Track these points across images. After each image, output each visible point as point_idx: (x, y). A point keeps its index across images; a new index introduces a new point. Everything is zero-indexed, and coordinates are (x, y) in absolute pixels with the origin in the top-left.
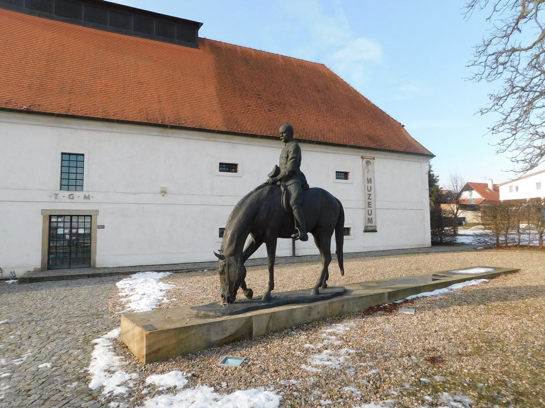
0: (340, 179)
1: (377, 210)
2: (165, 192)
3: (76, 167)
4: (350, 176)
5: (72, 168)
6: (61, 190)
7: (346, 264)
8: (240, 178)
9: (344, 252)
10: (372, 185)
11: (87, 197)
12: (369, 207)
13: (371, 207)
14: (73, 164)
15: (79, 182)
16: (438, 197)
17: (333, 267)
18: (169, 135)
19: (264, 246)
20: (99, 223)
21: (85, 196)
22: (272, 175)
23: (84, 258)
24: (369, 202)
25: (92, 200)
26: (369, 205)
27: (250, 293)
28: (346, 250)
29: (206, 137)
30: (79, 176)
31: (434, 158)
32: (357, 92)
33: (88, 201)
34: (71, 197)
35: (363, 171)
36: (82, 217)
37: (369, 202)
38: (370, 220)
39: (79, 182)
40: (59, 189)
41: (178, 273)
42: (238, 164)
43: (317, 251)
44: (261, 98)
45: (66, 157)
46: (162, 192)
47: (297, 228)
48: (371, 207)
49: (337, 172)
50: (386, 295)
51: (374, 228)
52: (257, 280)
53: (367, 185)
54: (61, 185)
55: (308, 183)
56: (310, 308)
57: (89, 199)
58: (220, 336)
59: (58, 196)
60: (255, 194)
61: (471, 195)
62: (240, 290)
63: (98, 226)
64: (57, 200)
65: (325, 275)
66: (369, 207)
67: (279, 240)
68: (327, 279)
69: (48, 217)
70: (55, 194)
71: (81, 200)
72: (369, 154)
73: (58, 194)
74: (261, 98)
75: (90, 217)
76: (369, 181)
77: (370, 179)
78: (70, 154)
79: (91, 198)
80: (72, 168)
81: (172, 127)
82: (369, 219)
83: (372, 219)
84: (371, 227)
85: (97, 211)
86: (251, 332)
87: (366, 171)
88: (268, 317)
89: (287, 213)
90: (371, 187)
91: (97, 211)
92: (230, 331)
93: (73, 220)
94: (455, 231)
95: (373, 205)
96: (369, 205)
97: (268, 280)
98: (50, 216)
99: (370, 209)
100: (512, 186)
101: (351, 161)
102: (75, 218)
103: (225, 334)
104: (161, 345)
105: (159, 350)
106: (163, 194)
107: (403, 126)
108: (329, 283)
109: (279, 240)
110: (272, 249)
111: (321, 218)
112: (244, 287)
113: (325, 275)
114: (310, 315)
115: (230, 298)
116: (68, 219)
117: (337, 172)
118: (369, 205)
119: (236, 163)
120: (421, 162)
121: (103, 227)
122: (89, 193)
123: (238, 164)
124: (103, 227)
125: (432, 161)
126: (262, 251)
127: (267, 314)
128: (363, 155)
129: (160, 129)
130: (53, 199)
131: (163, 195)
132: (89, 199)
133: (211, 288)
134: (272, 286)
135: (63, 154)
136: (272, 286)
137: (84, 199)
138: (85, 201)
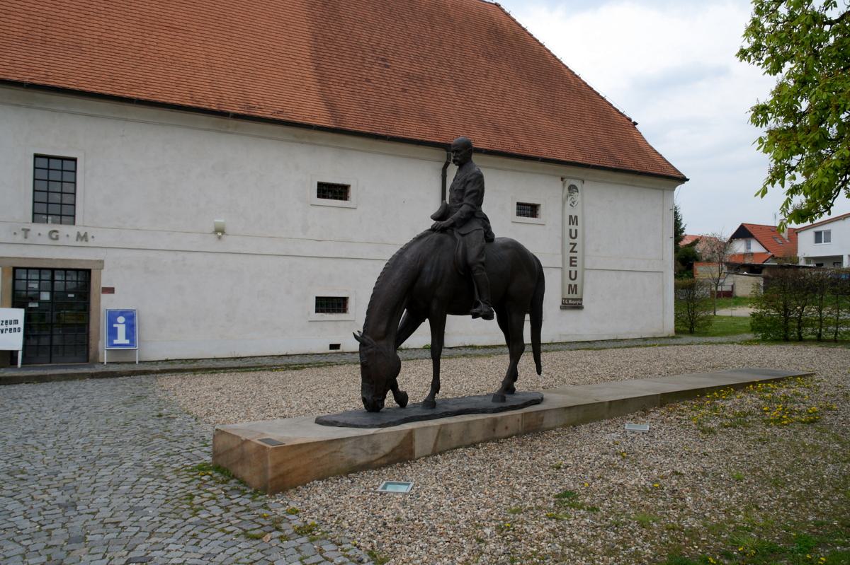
0: (524, 215)
1: (586, 272)
2: (223, 232)
3: (62, 182)
4: (542, 211)
5: (54, 187)
6: (33, 222)
7: (544, 357)
8: (353, 210)
9: (542, 341)
10: (579, 228)
11: (84, 237)
12: (571, 265)
13: (576, 266)
14: (55, 176)
15: (66, 210)
16: (686, 258)
17: (526, 360)
18: (230, 130)
19: (425, 327)
20: (105, 284)
21: (79, 235)
22: (438, 216)
23: (38, 346)
24: (571, 258)
25: (91, 243)
26: (572, 262)
27: (402, 399)
28: (545, 337)
29: (295, 136)
30: (67, 199)
31: (686, 182)
32: (557, 59)
33: (84, 243)
34: (54, 235)
35: (564, 203)
36: (46, 271)
37: (571, 258)
38: (573, 289)
39: (66, 210)
40: (31, 220)
41: (248, 371)
42: (349, 186)
43: (500, 338)
44: (388, 67)
45: (43, 163)
46: (216, 231)
47: (478, 300)
48: (576, 266)
49: (518, 204)
50: (607, 405)
51: (579, 302)
52: (413, 379)
53: (568, 227)
54: (34, 214)
55: (493, 230)
56: (495, 421)
57: (87, 241)
58: (369, 457)
59: (29, 233)
60: (414, 248)
61: (748, 247)
62: (390, 394)
63: (103, 288)
64: (27, 241)
65: (513, 375)
66: (571, 265)
67: (449, 317)
68: (515, 379)
69: (11, 270)
70: (23, 230)
71: (72, 241)
72: (574, 177)
73: (28, 230)
74: (388, 67)
75: (17, 270)
76: (573, 220)
77: (576, 217)
78: (49, 157)
79: (90, 240)
80: (54, 187)
81: (237, 116)
82: (570, 286)
83: (576, 286)
84: (573, 299)
85: (102, 262)
86: (412, 452)
87: (568, 203)
88: (436, 431)
89: (462, 274)
90: (576, 231)
91: (102, 262)
92: (386, 448)
93: (57, 277)
94: (799, 334)
95: (579, 262)
96: (571, 262)
97: (430, 379)
98: (15, 269)
99: (573, 269)
100: (820, 232)
101: (543, 189)
102: (58, 274)
103: (377, 453)
104: (290, 466)
105: (288, 472)
106: (220, 234)
107: (635, 124)
108: (518, 385)
109: (449, 317)
110: (438, 332)
111: (510, 289)
112: (394, 387)
113: (513, 375)
114: (494, 430)
115: (373, 405)
116: (47, 276)
117: (518, 204)
118: (572, 262)
119: (346, 183)
120: (663, 190)
121: (110, 290)
122: (87, 230)
123: (349, 186)
124: (110, 290)
125: (680, 190)
126: (422, 336)
127: (434, 427)
128: (563, 175)
129: (213, 119)
130: (20, 238)
131: (220, 237)
132: (87, 241)
133: (346, 388)
134: (436, 386)
135: (36, 156)
136: (436, 386)
137: (77, 240)
138: (79, 243)
